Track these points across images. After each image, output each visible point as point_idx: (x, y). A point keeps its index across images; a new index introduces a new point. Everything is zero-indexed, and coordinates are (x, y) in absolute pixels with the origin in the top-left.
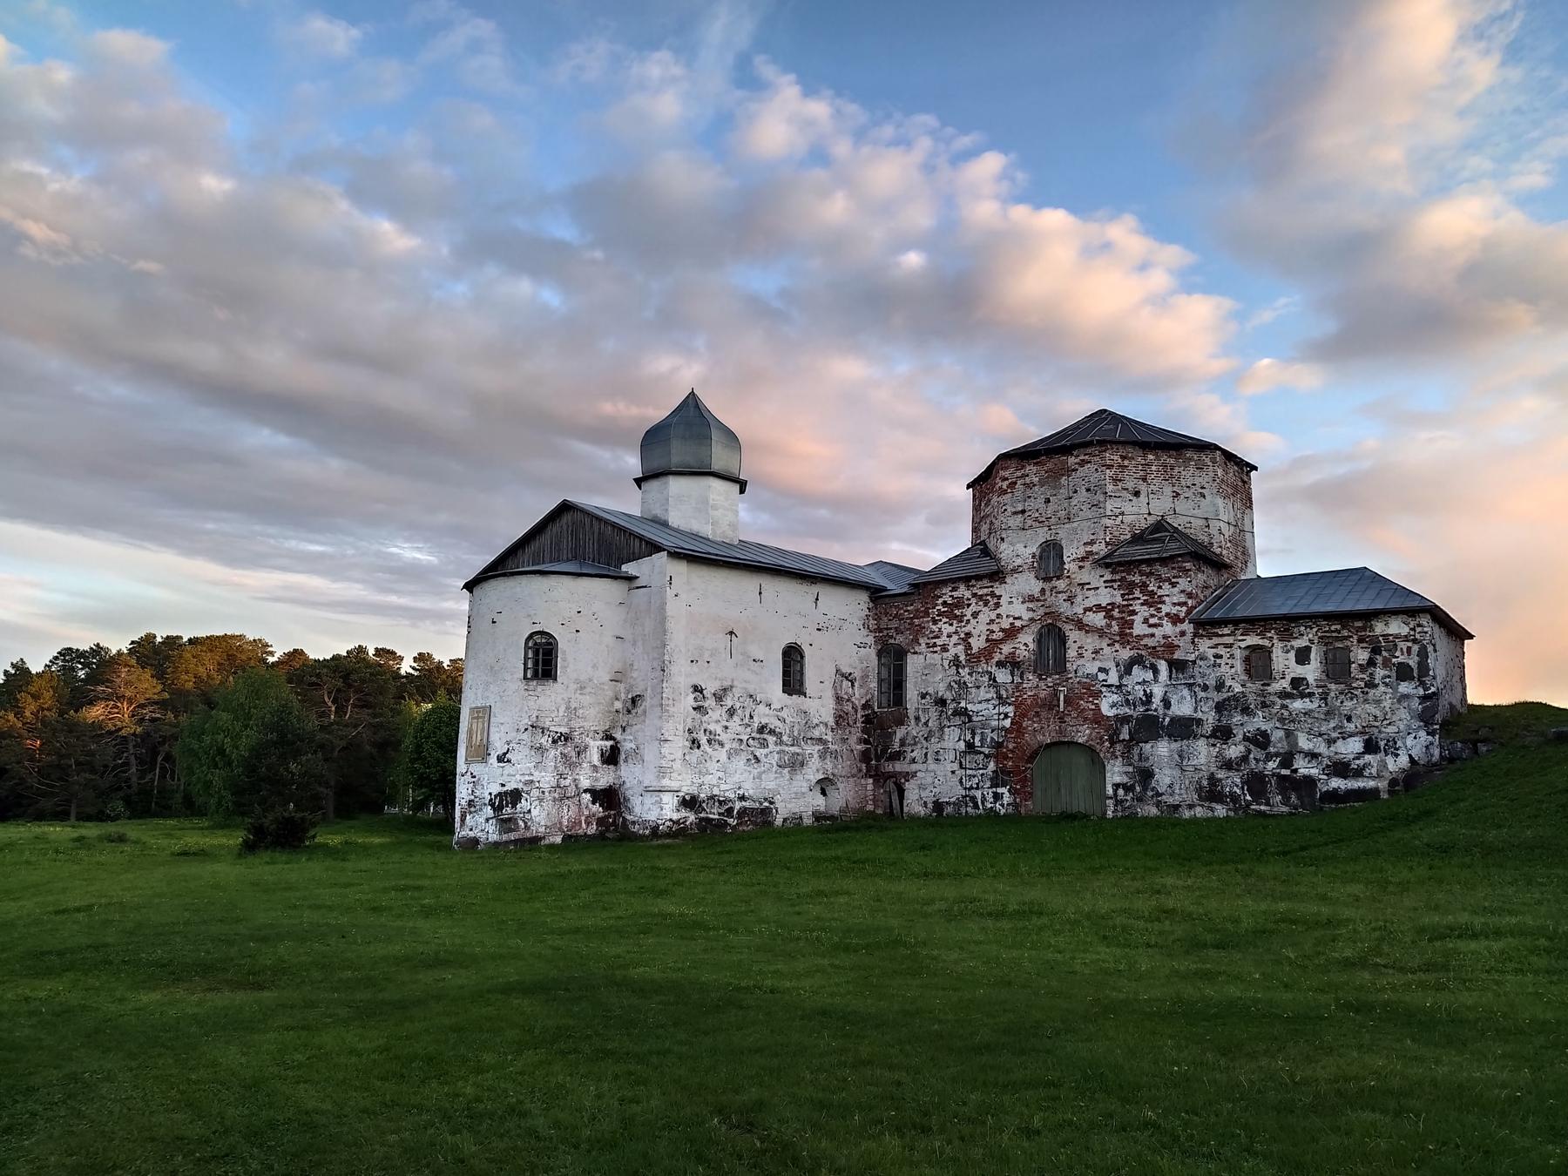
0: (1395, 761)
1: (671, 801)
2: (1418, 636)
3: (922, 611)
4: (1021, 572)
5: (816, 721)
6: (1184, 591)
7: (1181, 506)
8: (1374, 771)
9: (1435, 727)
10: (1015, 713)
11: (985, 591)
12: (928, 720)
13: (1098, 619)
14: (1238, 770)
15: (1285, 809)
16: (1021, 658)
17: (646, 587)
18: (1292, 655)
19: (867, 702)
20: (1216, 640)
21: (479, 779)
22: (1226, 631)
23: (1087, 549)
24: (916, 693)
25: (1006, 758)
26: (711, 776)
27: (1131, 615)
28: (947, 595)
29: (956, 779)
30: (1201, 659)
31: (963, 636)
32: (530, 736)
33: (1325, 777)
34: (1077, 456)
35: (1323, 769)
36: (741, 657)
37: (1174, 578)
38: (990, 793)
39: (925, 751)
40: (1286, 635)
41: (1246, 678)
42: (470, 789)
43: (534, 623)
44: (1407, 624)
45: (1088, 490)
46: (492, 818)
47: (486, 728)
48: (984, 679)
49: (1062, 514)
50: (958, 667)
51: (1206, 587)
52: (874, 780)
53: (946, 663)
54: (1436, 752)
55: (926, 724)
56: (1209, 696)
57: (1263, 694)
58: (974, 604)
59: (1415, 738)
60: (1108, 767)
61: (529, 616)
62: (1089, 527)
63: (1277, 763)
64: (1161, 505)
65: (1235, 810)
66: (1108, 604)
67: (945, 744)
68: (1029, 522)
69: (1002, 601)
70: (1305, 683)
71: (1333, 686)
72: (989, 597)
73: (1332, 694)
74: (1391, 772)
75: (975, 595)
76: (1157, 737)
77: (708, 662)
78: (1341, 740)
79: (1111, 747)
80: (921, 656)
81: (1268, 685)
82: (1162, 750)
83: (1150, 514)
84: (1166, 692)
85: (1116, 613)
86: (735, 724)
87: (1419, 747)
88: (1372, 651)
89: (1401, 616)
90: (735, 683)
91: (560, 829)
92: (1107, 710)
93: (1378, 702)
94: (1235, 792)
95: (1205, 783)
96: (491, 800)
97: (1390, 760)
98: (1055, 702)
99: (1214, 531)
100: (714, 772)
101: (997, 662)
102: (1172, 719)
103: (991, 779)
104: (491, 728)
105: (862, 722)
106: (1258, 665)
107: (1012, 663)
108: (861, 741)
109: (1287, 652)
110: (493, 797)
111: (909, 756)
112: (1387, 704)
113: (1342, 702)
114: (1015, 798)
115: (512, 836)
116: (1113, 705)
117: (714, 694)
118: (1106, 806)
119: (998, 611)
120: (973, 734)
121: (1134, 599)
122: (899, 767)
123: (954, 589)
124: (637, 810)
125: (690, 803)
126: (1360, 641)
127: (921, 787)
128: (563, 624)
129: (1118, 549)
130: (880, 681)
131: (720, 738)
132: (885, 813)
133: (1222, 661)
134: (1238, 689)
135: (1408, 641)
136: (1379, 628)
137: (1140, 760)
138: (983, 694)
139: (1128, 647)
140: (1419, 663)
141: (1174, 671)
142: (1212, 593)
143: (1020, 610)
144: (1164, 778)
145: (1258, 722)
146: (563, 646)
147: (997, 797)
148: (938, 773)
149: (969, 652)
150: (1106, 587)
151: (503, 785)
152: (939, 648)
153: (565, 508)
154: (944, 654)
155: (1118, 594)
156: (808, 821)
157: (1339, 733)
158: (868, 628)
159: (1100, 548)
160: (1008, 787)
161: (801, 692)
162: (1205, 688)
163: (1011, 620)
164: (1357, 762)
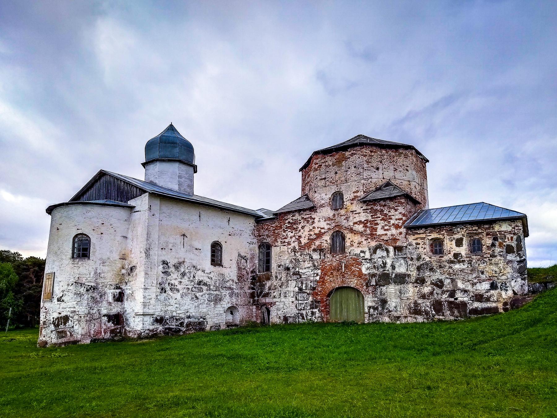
0: (506, 293)
1: (149, 320)
2: (516, 231)
3: (279, 227)
4: (324, 207)
5: (227, 279)
6: (401, 213)
7: (398, 175)
8: (495, 299)
9: (525, 276)
10: (321, 273)
11: (307, 216)
12: (281, 278)
13: (360, 228)
14: (428, 299)
15: (452, 318)
16: (324, 247)
17: (138, 211)
18: (454, 242)
19: (253, 270)
20: (416, 236)
21: (48, 310)
22: (421, 231)
23: (355, 195)
24: (276, 265)
25: (317, 294)
26: (172, 307)
27: (376, 225)
28: (290, 218)
29: (294, 306)
30: (409, 245)
31: (297, 237)
32: (74, 287)
33: (471, 302)
34: (350, 152)
35: (470, 298)
36: (189, 247)
37: (396, 207)
38: (310, 312)
39: (280, 292)
40: (451, 232)
41: (431, 254)
42: (44, 316)
43: (78, 229)
44: (511, 226)
45: (355, 167)
46: (54, 331)
47: (52, 284)
48: (307, 257)
50: (295, 252)
51: (410, 212)
52: (256, 307)
53: (290, 250)
54: (526, 288)
55: (280, 279)
56: (413, 263)
57: (439, 261)
58: (302, 222)
59: (516, 281)
60: (366, 299)
62: (356, 185)
64: (389, 174)
65: (427, 319)
66: (365, 221)
67: (289, 289)
68: (328, 183)
69: (316, 221)
70: (460, 255)
71: (474, 257)
72: (309, 219)
73: (474, 261)
74: (504, 299)
76: (389, 283)
77: (171, 249)
78: (479, 283)
79: (367, 289)
80: (278, 248)
81: (442, 257)
82: (391, 290)
83: (384, 178)
84: (393, 262)
85: (368, 225)
86: (185, 281)
87: (517, 286)
88: (493, 239)
89: (508, 222)
90: (186, 260)
91: (89, 336)
92: (364, 271)
94: (427, 310)
95: (412, 305)
96: (53, 321)
97: (503, 293)
98: (340, 268)
99: (412, 187)
100: (174, 304)
101: (313, 249)
102: (396, 275)
103: (311, 305)
104: (54, 284)
105: (251, 279)
107: (320, 250)
108: (250, 288)
109: (452, 241)
110: (54, 320)
111: (273, 295)
112: (501, 265)
113: (479, 265)
114: (322, 314)
115: (63, 340)
116: (368, 269)
117: (174, 266)
118: (364, 317)
119: (313, 225)
120: (302, 283)
121: (377, 217)
122: (268, 300)
123: (293, 216)
124: (132, 325)
125: (160, 320)
126: (488, 234)
127: (278, 310)
128: (93, 230)
129: (369, 194)
130: (260, 260)
131: (177, 288)
132: (261, 322)
133: (420, 246)
134: (428, 259)
135: (511, 234)
136: (497, 228)
137: (381, 295)
138: (307, 264)
139: (375, 241)
140: (517, 245)
142: (413, 215)
143: (323, 224)
144: (392, 303)
145: (437, 276)
146: (93, 240)
147: (313, 313)
148: (286, 303)
149: (300, 245)
150: (364, 212)
151: (60, 313)
152: (287, 243)
153: (102, 174)
154: (289, 246)
155: (369, 215)
156: (223, 327)
157: (478, 280)
158: (254, 235)
159: (361, 194)
160: (318, 309)
161: (220, 265)
162: (412, 259)
164: (487, 294)
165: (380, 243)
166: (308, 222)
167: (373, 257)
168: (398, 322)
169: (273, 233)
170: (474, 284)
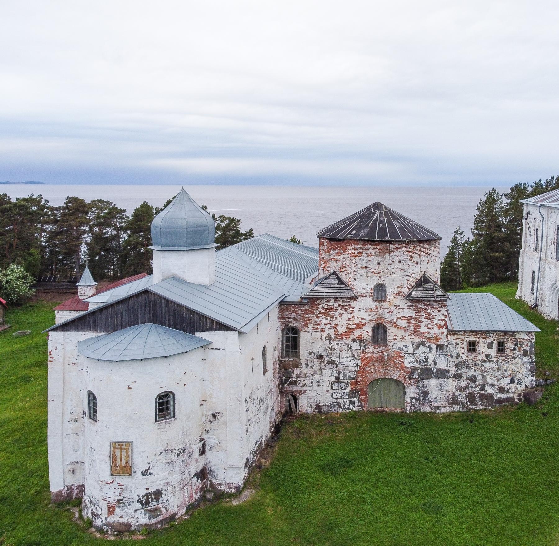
3: (310, 311)
8: (513, 391)
11: (345, 304)
13: (404, 323)
15: (482, 407)
20: (456, 337)
29: (329, 395)
30: (450, 344)
31: (333, 325)
45: (400, 262)
49: (387, 271)
50: (330, 340)
54: (534, 383)
55: (312, 367)
59: (528, 378)
61: (157, 383)
63: (479, 388)
69: (355, 310)
70: (490, 356)
71: (500, 358)
75: (339, 305)
76: (431, 377)
82: (432, 384)
83: (421, 272)
85: (412, 321)
87: (529, 381)
92: (407, 364)
93: (516, 364)
94: (463, 401)
95: (451, 397)
96: (139, 499)
97: (519, 386)
102: (437, 370)
106: (472, 347)
111: (302, 383)
112: (519, 365)
113: (503, 364)
115: (159, 519)
119: (353, 314)
134: (465, 358)
135: (527, 341)
137: (423, 387)
139: (418, 337)
141: (439, 349)
144: (433, 395)
145: (472, 372)
147: (351, 402)
148: (319, 391)
150: (408, 309)
151: (147, 489)
154: (322, 333)
162: (451, 357)
163: (360, 319)
164: (507, 387)
165: (423, 340)
166: (346, 311)
167: (416, 352)
168: (438, 411)
169: (302, 317)
170: (499, 380)
